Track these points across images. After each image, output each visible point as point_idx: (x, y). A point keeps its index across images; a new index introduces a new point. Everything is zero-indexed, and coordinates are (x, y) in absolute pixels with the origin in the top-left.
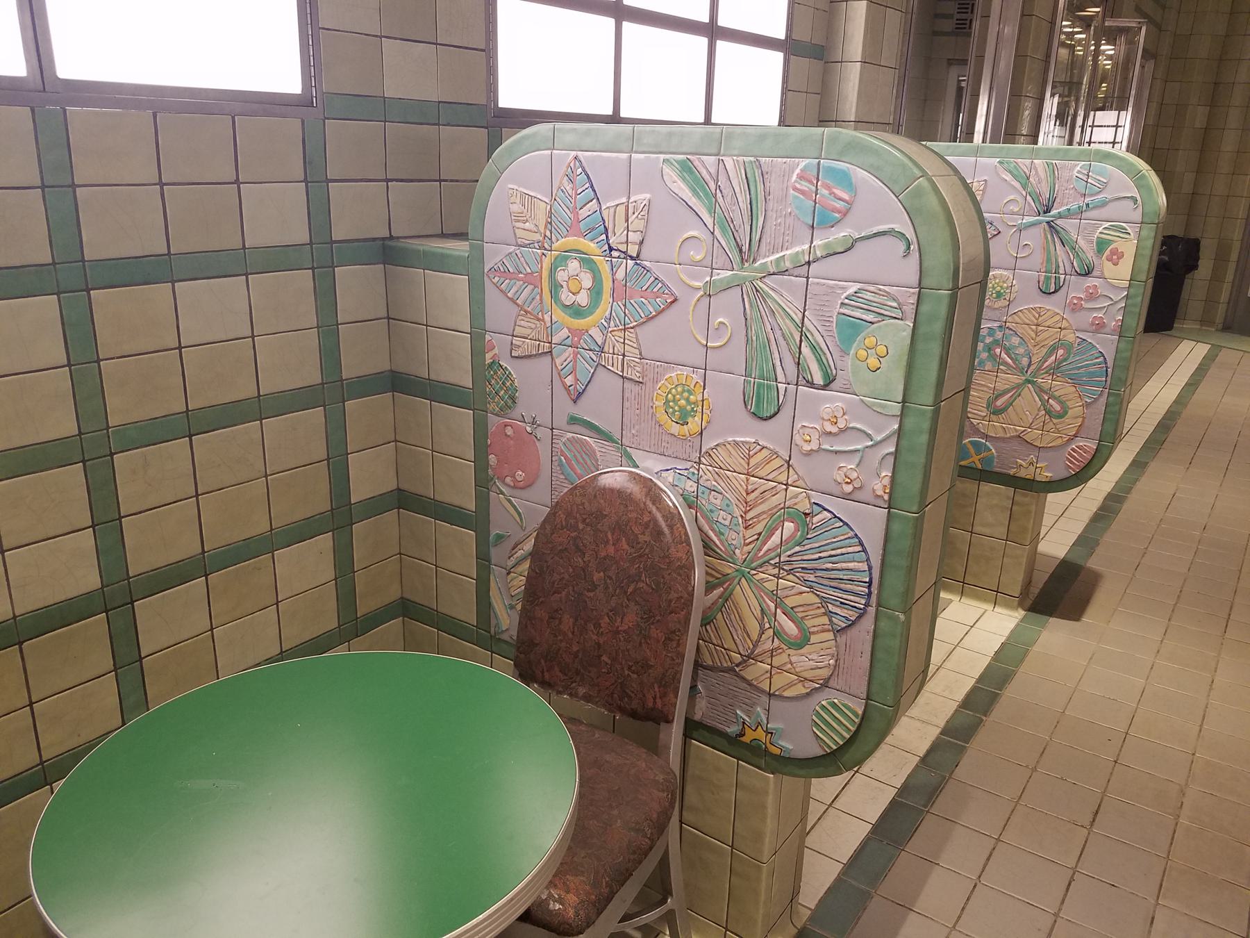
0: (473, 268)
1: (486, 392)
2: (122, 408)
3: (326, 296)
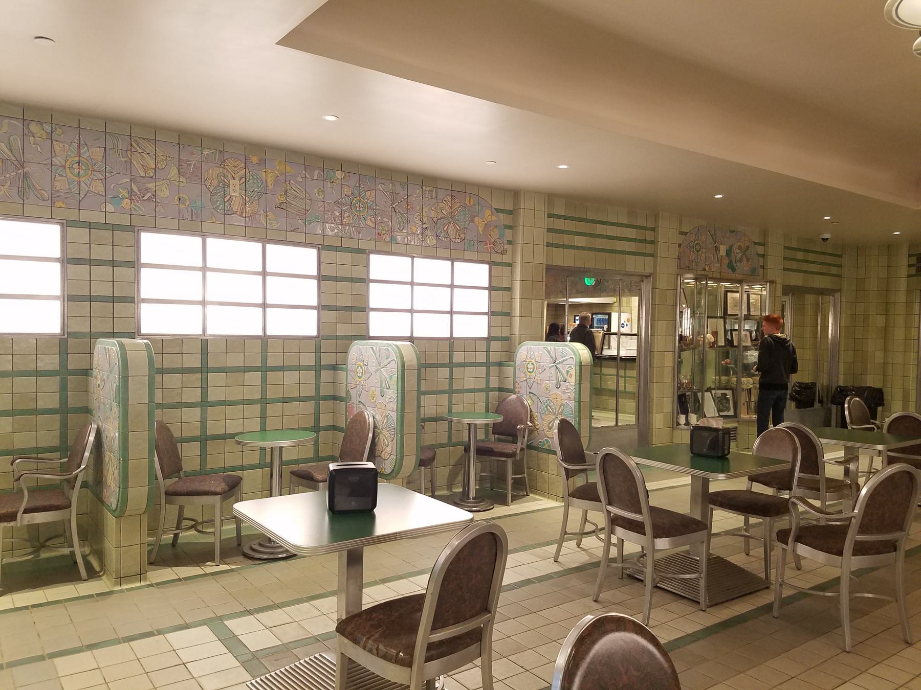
0: (346, 370)
1: (346, 399)
2: (270, 395)
3: (318, 376)
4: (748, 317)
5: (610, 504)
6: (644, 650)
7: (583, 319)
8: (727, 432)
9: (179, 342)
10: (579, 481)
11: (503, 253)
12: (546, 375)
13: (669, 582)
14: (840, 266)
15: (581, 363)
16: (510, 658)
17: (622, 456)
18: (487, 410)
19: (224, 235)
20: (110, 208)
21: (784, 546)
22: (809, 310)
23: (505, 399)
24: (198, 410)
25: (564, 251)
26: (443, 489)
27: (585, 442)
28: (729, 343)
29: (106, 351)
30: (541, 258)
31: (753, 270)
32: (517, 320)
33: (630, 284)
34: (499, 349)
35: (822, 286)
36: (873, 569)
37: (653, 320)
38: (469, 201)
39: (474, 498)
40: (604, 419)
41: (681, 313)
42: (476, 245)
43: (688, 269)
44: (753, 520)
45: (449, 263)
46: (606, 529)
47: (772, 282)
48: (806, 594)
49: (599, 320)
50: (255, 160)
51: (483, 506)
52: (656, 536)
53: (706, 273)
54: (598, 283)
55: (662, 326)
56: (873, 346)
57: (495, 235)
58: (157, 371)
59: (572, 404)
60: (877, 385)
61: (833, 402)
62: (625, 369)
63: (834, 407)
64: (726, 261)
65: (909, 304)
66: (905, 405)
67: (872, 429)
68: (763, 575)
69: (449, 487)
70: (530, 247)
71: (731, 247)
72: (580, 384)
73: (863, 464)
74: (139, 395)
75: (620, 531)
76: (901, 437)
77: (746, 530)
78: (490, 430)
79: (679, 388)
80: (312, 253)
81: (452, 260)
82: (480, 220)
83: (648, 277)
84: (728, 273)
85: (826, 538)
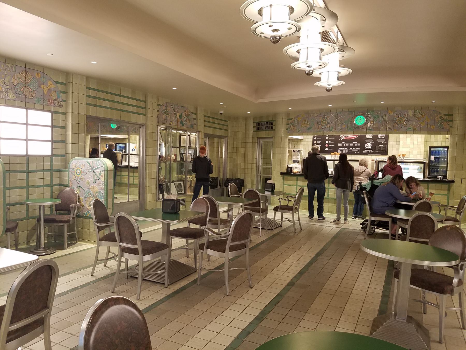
4: (190, 148)
5: (121, 242)
6: (129, 311)
7: (110, 146)
8: (178, 201)
10: (106, 232)
11: (60, 106)
12: (88, 176)
13: (149, 277)
14: (227, 126)
15: (107, 169)
16: (64, 330)
17: (128, 217)
18: (52, 197)
21: (202, 251)
22: (215, 145)
23: (63, 190)
25: (98, 109)
26: (24, 245)
27: (109, 212)
28: (182, 159)
30: (83, 111)
32: (69, 146)
33: (135, 128)
34: (58, 163)
35: (220, 134)
36: (238, 257)
37: (146, 147)
38: (38, 75)
39: (44, 248)
40: (122, 198)
41: (160, 144)
42: (42, 101)
43: (162, 123)
44: (190, 241)
45: (25, 110)
46: (119, 256)
47: (199, 132)
48: (213, 272)
49: (120, 147)
51: (49, 251)
52: (144, 254)
53: (171, 126)
54: (118, 127)
55: (150, 150)
56: (240, 161)
57: (55, 97)
59: (103, 192)
60: (242, 178)
61: (225, 186)
62: (134, 172)
63: (225, 187)
64: (180, 121)
65: (253, 143)
66: (252, 187)
67: (238, 197)
68: (194, 266)
69: (28, 243)
71: (182, 114)
72: (107, 180)
73: (235, 211)
75: (126, 255)
76: (249, 200)
77: (187, 246)
78: (54, 208)
79: (159, 181)
81: (27, 109)
82: (45, 87)
83: (143, 125)
84: (180, 126)
85: (218, 245)
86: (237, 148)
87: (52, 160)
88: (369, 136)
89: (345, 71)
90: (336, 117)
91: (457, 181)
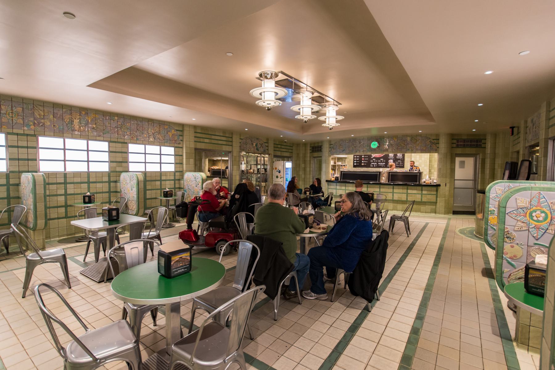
9: (55, 174)
11: (179, 144)
19: (72, 138)
20: (26, 128)
24: (64, 197)
29: (26, 178)
30: (192, 145)
31: (264, 151)
32: (185, 166)
34: (178, 176)
43: (243, 150)
50: (84, 113)
55: (235, 167)
57: (176, 138)
58: (46, 184)
65: (310, 160)
70: (189, 142)
74: (40, 190)
80: (107, 143)
84: (256, 151)
86: (299, 165)
87: (175, 174)
88: (391, 155)
89: (340, 118)
90: (360, 143)
91: (443, 185)
